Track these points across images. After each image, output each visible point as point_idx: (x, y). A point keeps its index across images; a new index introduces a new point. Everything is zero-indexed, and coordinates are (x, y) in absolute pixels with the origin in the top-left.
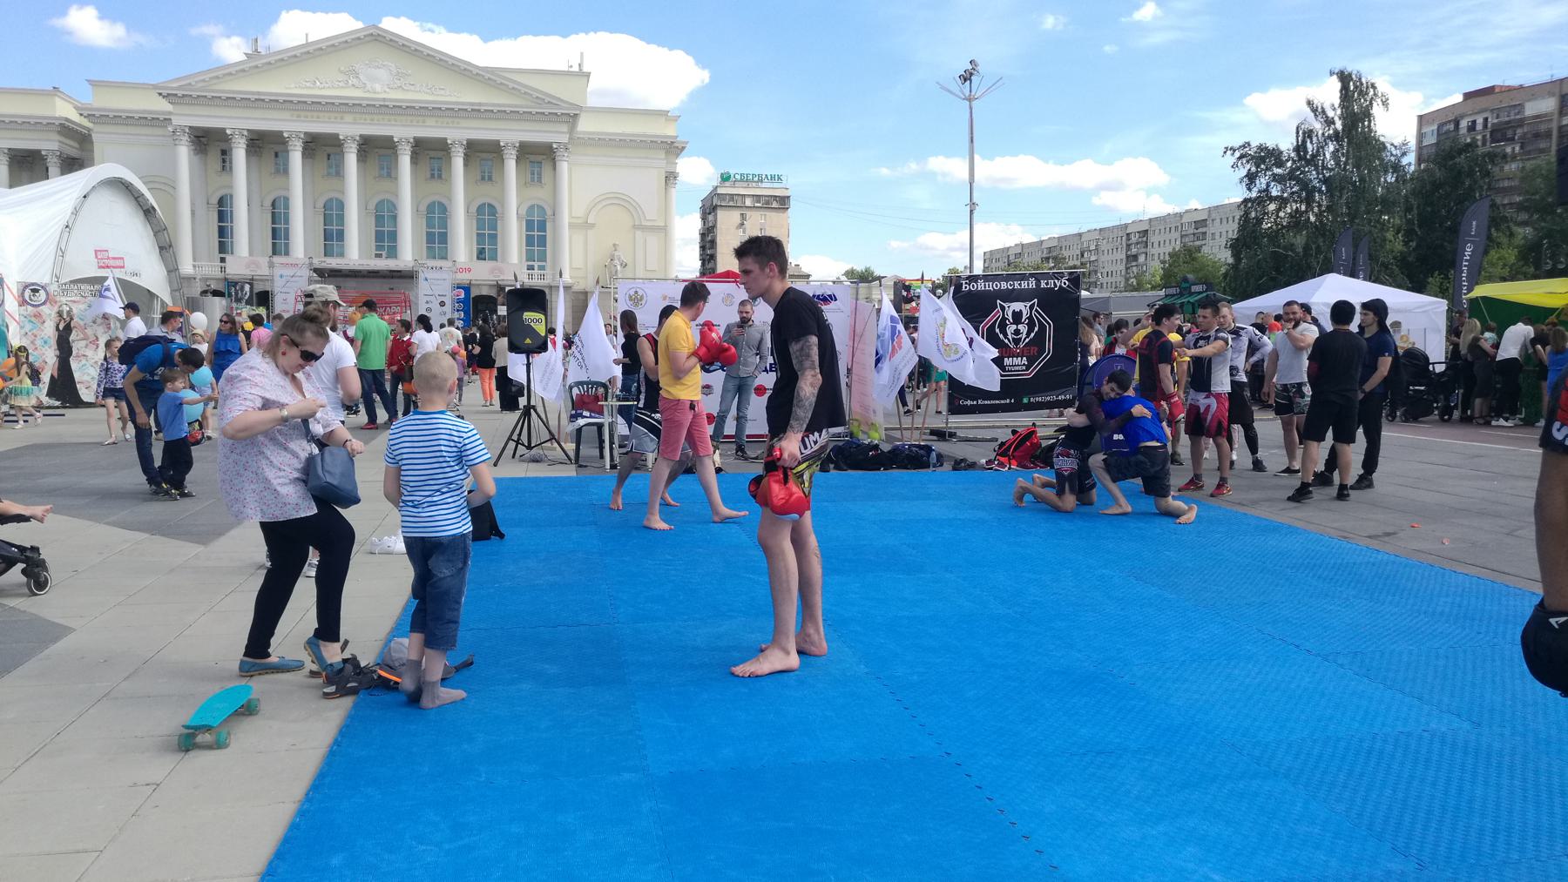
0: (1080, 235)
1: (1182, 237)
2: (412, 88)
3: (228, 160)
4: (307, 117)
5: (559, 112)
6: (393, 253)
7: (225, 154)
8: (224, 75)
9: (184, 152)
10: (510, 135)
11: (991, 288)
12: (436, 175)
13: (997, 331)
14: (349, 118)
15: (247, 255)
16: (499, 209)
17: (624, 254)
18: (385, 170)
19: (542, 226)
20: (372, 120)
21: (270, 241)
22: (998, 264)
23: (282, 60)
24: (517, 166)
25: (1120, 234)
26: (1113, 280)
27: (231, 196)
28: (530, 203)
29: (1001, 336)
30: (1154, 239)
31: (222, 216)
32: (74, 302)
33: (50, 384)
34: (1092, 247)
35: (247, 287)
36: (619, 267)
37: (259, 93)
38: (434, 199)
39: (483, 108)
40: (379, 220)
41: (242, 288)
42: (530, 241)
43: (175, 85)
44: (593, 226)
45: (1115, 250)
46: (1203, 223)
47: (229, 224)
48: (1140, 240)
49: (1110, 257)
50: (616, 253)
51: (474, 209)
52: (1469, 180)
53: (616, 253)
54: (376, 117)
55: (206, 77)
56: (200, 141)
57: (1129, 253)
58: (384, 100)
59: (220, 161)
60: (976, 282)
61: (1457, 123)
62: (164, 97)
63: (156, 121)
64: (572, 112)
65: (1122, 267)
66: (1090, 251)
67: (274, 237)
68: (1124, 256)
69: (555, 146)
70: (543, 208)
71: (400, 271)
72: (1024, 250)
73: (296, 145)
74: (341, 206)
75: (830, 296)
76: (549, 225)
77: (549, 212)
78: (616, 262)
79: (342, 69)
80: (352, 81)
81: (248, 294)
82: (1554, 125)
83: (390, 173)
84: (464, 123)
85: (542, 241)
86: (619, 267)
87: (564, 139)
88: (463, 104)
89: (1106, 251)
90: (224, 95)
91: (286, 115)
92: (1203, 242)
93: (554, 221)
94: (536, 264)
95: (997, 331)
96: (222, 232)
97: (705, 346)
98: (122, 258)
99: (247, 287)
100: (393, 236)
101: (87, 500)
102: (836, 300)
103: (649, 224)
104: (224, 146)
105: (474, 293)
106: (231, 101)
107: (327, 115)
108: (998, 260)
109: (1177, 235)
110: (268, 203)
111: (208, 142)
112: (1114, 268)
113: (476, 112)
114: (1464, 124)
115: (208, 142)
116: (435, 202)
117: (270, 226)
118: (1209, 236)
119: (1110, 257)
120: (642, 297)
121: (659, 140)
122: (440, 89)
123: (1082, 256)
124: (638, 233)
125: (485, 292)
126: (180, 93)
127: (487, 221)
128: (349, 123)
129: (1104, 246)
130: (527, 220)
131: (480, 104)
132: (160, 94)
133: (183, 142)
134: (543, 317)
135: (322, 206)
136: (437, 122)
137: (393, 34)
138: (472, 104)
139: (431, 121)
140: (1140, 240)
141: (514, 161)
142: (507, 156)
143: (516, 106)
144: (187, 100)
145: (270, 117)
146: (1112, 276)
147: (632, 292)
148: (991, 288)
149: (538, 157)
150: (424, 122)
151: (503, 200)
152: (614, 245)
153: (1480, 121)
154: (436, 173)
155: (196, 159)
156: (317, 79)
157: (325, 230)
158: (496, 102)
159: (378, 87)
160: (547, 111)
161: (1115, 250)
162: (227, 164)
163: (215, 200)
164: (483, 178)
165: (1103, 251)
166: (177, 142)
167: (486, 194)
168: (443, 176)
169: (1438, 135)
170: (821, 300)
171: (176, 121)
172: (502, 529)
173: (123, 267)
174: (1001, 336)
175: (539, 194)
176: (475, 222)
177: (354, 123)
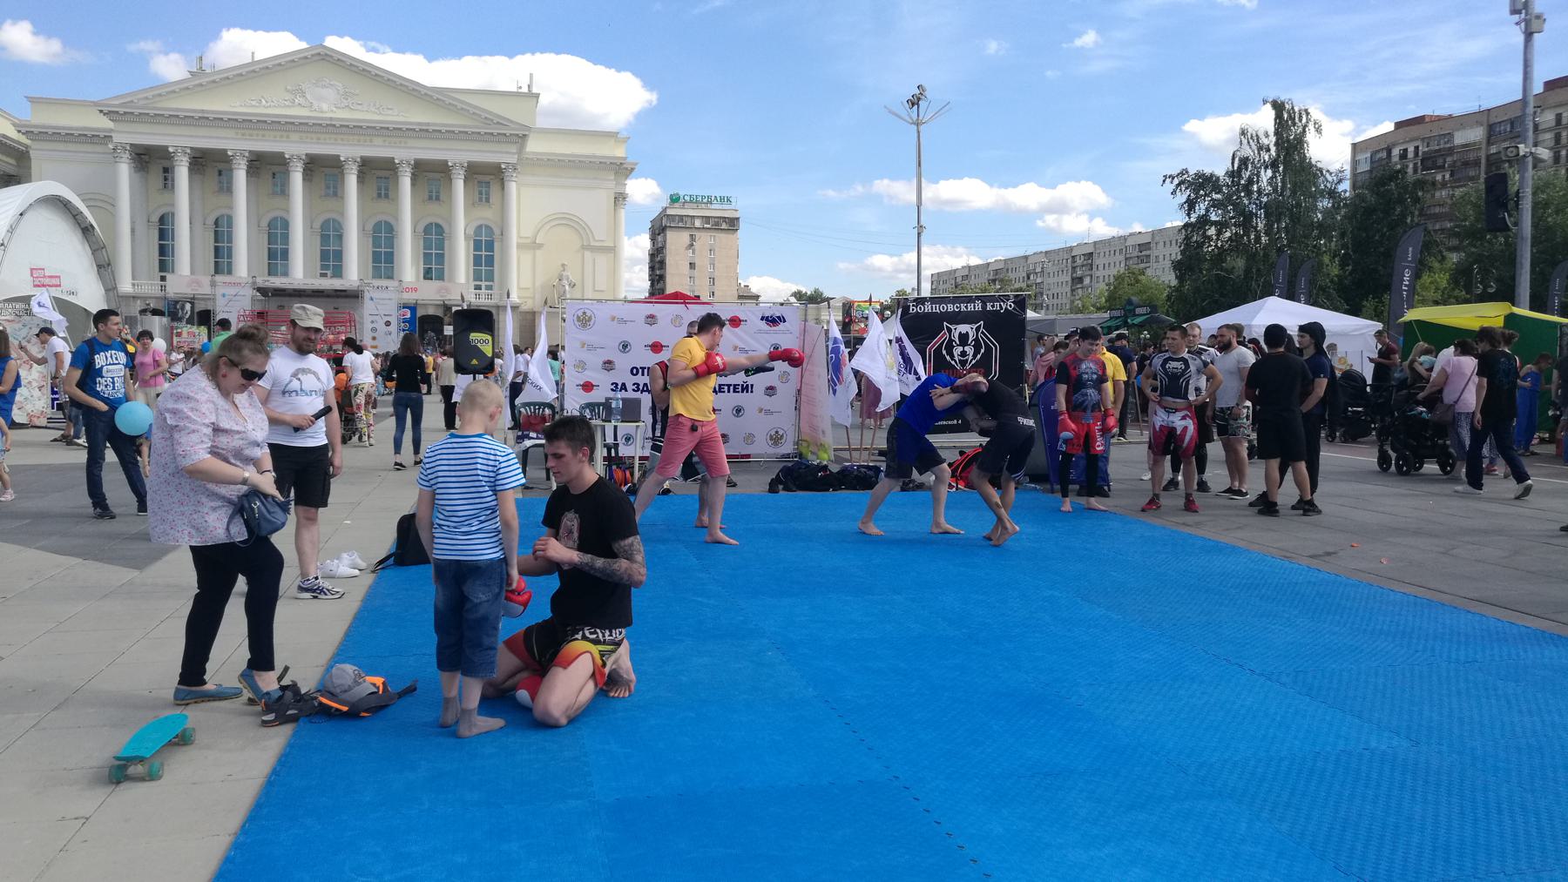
0: (1026, 258)
1: (1126, 259)
2: (359, 107)
3: (170, 178)
4: (251, 135)
5: (508, 132)
6: (338, 272)
7: (168, 172)
9: (124, 170)
10: (458, 155)
11: (938, 311)
12: (484, 199)
13: (944, 352)
14: (295, 137)
16: (446, 229)
17: (572, 274)
18: (332, 189)
19: (490, 246)
20: (342, 140)
21: (212, 260)
22: (945, 286)
24: (465, 187)
26: (1059, 302)
27: (173, 214)
29: (948, 358)
30: (1098, 261)
31: (163, 235)
32: (9, 321)
34: (1039, 270)
35: (188, 306)
36: (567, 287)
37: (203, 111)
39: (431, 128)
41: (183, 308)
42: (477, 261)
43: (117, 102)
45: (1060, 272)
46: (1144, 247)
47: (170, 242)
49: (1056, 279)
50: (565, 274)
51: (421, 228)
53: (565, 274)
54: (323, 136)
55: (149, 95)
56: (142, 159)
57: (1074, 275)
58: (331, 119)
59: (162, 178)
60: (923, 304)
61: (1389, 151)
62: (105, 114)
63: (96, 139)
64: (520, 133)
65: (1068, 289)
66: (1036, 273)
67: (216, 256)
68: (1069, 279)
70: (491, 228)
71: (345, 291)
73: (240, 164)
75: (779, 317)
76: (496, 245)
77: (497, 231)
78: (565, 282)
79: (288, 87)
80: (302, 100)
81: (189, 313)
82: (1483, 155)
83: (335, 190)
84: (411, 143)
85: (490, 261)
86: (567, 287)
87: (513, 159)
90: (167, 113)
91: (231, 133)
92: (1148, 265)
93: (502, 241)
94: (483, 284)
95: (944, 352)
96: (163, 250)
98: (59, 277)
99: (188, 306)
102: (785, 321)
104: (166, 164)
106: (175, 119)
107: (272, 133)
109: (1122, 258)
110: (211, 221)
112: (1058, 290)
113: (424, 132)
114: (1396, 152)
115: (151, 161)
116: (432, 224)
117: (211, 244)
118: (1153, 258)
119: (1056, 279)
120: (590, 318)
122: (388, 109)
123: (1029, 278)
124: (588, 254)
125: (431, 311)
126: (121, 110)
127: (434, 243)
130: (474, 240)
131: (428, 124)
132: (101, 111)
133: (123, 160)
134: (490, 338)
135: (157, 220)
136: (385, 141)
138: (419, 124)
139: (378, 141)
142: (455, 176)
143: (465, 126)
144: (128, 117)
147: (580, 313)
148: (938, 311)
150: (405, 143)
151: (397, 216)
152: (563, 265)
153: (1411, 149)
154: (383, 192)
156: (262, 97)
157: (269, 249)
159: (325, 106)
160: (495, 132)
161: (1060, 272)
162: (170, 182)
163: (155, 218)
164: (430, 198)
166: (117, 160)
167: (434, 213)
168: (441, 198)
169: (1372, 162)
170: (770, 321)
171: (117, 138)
173: (60, 286)
174: (948, 358)
175: (487, 215)
176: (371, 240)
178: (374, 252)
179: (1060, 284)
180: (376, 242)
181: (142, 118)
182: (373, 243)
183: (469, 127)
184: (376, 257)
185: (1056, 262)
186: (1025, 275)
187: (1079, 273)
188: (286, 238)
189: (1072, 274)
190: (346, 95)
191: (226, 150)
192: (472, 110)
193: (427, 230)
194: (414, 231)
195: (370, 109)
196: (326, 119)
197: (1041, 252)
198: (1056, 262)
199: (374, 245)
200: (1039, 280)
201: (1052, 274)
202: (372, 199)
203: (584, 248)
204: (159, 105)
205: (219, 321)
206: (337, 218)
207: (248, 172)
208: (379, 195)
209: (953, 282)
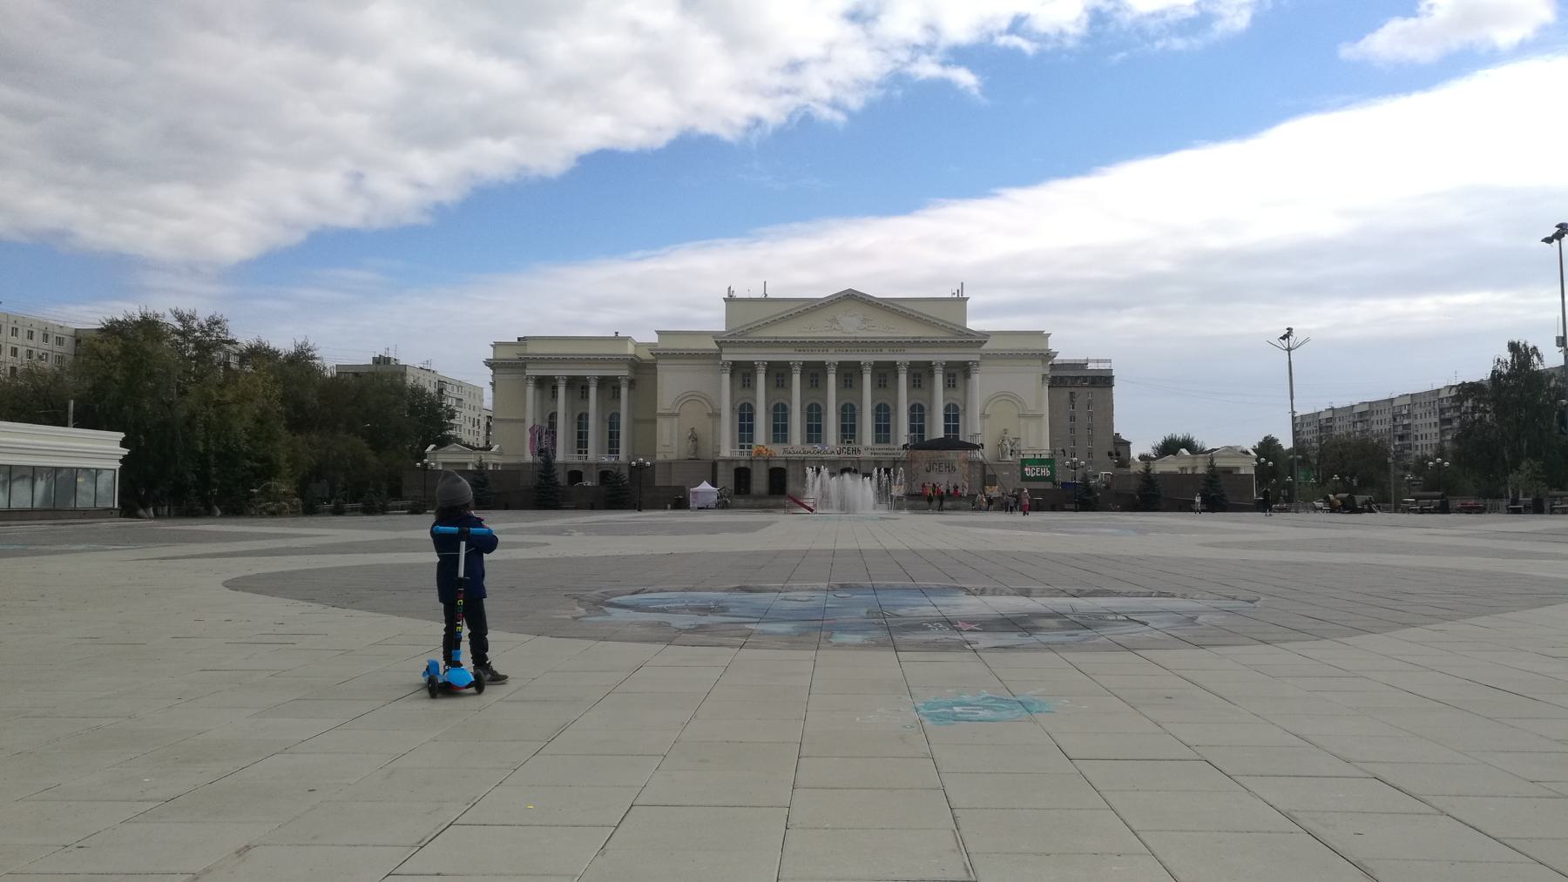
0: (1391, 400)
5: (974, 340)
7: (555, 388)
8: (756, 327)
9: (530, 390)
10: (938, 357)
14: (832, 351)
15: (799, 443)
22: (1309, 429)
23: (775, 320)
25: (1432, 399)
26: (1428, 442)
28: (610, 413)
33: (395, 552)
38: (812, 402)
39: (922, 340)
40: (742, 418)
42: (844, 428)
44: (988, 416)
45: (1428, 414)
48: (1453, 404)
49: (1424, 421)
52: (163, 342)
53: (1006, 436)
55: (745, 329)
57: (1443, 416)
58: (856, 338)
65: (1437, 430)
66: (1403, 415)
68: (1437, 420)
69: (756, 363)
72: (1336, 416)
74: (619, 415)
76: (961, 418)
77: (961, 408)
80: (836, 326)
83: (585, 395)
84: (908, 350)
85: (887, 429)
87: (977, 358)
88: (908, 338)
89: (1419, 416)
91: (792, 351)
93: (965, 414)
94: (746, 444)
96: (580, 435)
97: (941, 504)
100: (785, 428)
101: (1223, 617)
103: (1030, 413)
105: (773, 465)
108: (1309, 424)
111: (743, 373)
112: (1428, 431)
113: (917, 343)
115: (743, 373)
119: (1424, 421)
121: (1038, 353)
123: (1395, 420)
124: (1023, 421)
126: (728, 340)
127: (814, 420)
128: (887, 354)
129: (1418, 411)
131: (919, 338)
137: (862, 294)
138: (913, 338)
139: (885, 350)
140: (1453, 404)
141: (834, 375)
145: (781, 352)
146: (1426, 438)
149: (958, 373)
152: (1005, 430)
154: (848, 383)
155: (538, 392)
158: (937, 335)
161: (1428, 414)
162: (585, 395)
163: (547, 416)
165: (1416, 415)
172: (501, 672)
175: (956, 396)
177: (835, 354)
178: (808, 425)
179: (1428, 425)
180: (776, 418)
181: (742, 344)
182: (808, 418)
183: (947, 338)
184: (776, 428)
185: (1423, 404)
186: (1390, 416)
187: (1448, 415)
188: (751, 417)
189: (1440, 416)
190: (864, 320)
191: (753, 362)
192: (949, 326)
193: (844, 408)
194: (767, 409)
195: (883, 329)
196: (852, 338)
197: (1408, 395)
198: (1423, 404)
199: (774, 421)
200: (1406, 422)
201: (1419, 416)
202: (1044, 377)
203: (1019, 416)
204: (749, 336)
205: (713, 486)
206: (750, 402)
207: (598, 387)
208: (778, 386)
209: (1318, 425)
